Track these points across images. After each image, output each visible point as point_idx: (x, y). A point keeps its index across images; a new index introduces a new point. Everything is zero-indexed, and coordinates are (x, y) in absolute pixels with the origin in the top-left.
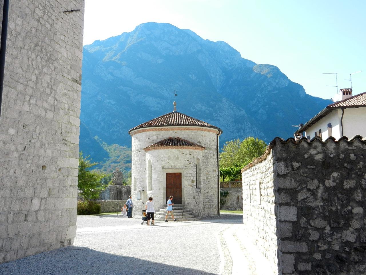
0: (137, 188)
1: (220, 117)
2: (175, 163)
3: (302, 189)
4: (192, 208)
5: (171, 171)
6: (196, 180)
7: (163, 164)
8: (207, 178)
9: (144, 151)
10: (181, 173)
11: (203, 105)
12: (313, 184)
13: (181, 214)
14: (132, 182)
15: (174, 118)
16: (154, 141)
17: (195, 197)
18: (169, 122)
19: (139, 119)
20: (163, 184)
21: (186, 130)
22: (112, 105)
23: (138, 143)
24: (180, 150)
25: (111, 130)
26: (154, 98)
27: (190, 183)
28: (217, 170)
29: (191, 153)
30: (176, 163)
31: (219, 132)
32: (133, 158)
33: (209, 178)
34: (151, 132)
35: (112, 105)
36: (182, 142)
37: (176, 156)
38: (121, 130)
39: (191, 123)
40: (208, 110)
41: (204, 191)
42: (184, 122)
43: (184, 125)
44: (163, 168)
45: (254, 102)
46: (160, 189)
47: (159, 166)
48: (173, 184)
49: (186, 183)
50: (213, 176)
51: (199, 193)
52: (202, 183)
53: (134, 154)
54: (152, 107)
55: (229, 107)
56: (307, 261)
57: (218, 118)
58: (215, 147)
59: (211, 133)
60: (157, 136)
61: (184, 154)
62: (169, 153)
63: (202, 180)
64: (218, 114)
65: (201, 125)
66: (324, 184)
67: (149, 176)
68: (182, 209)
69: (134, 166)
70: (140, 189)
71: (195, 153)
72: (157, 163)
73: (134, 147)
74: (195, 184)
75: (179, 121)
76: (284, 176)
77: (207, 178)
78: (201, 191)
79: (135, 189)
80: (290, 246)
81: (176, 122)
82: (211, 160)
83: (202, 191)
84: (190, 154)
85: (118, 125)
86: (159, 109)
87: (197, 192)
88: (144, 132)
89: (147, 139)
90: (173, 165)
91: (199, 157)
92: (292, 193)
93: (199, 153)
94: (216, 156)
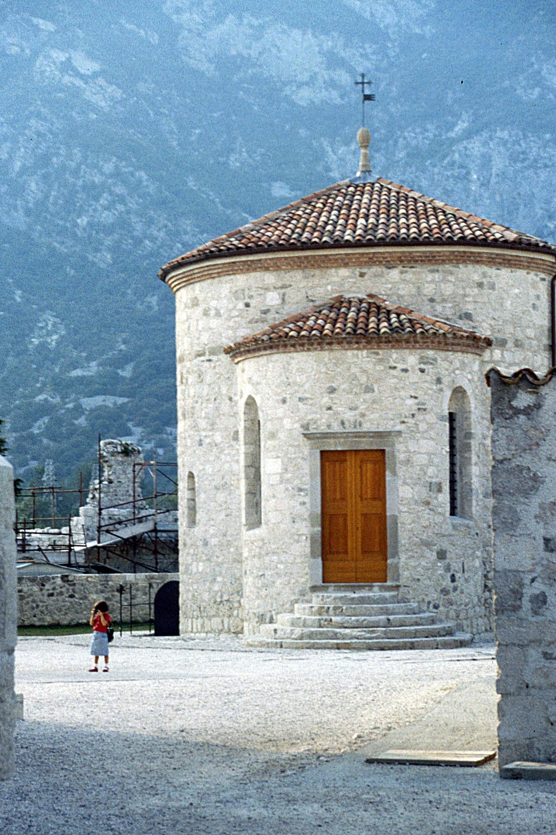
2: (356, 408)
6: (453, 482)
9: (225, 358)
10: (384, 451)
14: (180, 494)
16: (270, 316)
20: (307, 500)
21: (409, 261)
22: (82, 77)
23: (200, 323)
24: (380, 352)
25: (83, 221)
26: (310, 32)
30: (362, 408)
32: (183, 387)
34: (258, 274)
35: (82, 77)
38: (134, 219)
43: (396, 242)
47: (287, 424)
53: (184, 371)
54: (300, 85)
59: (521, 273)
61: (395, 368)
69: (188, 422)
71: (446, 365)
72: (281, 411)
73: (186, 340)
84: (422, 371)
85: (120, 190)
86: (342, 97)
89: (241, 305)
90: (349, 416)
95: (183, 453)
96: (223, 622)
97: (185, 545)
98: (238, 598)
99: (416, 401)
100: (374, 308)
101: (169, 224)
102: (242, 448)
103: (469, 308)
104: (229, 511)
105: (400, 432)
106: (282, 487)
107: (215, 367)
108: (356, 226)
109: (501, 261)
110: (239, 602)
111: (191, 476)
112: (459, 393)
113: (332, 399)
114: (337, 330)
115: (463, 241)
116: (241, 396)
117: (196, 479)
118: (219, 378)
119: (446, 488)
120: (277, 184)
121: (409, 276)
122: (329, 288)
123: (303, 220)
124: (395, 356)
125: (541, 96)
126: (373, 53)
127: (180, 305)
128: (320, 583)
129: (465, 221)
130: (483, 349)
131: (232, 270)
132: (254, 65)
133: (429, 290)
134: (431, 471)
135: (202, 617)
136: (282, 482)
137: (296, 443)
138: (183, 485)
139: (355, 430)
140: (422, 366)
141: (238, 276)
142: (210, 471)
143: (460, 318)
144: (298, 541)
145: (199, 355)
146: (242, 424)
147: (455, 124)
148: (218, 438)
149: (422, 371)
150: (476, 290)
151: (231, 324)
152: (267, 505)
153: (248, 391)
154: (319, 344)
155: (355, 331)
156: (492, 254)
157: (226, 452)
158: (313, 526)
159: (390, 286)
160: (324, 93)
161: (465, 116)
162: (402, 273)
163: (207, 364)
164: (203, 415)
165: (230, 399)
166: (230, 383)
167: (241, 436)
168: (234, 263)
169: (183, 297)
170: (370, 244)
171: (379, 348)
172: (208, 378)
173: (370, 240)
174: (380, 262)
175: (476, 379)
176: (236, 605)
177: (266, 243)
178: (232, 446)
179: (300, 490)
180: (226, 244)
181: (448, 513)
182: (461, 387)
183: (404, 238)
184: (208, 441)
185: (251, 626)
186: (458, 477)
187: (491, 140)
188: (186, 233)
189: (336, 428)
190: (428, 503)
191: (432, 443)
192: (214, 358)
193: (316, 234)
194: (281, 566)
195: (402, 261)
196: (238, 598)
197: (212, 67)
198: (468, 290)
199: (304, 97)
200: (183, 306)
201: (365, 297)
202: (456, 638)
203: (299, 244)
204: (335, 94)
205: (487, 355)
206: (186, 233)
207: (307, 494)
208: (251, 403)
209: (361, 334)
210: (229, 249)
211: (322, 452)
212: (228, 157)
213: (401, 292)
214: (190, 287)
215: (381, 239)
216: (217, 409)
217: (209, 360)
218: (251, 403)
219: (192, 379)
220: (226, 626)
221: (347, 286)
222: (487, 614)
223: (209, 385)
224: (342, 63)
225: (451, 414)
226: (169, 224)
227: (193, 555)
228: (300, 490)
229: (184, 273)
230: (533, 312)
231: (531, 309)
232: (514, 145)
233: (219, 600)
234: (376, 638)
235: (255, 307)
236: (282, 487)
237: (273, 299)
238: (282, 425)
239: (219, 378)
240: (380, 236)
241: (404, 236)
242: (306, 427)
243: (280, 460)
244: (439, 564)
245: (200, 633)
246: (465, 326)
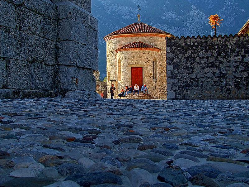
3: (176, 58)
11: (173, 13)
12: (180, 56)
13: (142, 96)
15: (138, 27)
18: (134, 30)
36: (143, 45)
39: (150, 31)
42: (145, 30)
43: (144, 32)
44: (129, 64)
45: (223, 9)
49: (146, 75)
55: (198, 14)
56: (176, 86)
57: (188, 25)
62: (134, 53)
66: (184, 56)
75: (141, 30)
76: (169, 53)
80: (170, 80)
81: (139, 30)
84: (149, 54)
89: (118, 43)
92: (172, 60)
93: (156, 54)
119: (153, 74)
125: (166, 18)
127: (107, 43)
133: (150, 41)
138: (107, 74)
149: (149, 54)
186: (155, 72)
198: (157, 41)
199: (125, 18)
208: (119, 59)
211: (132, 68)
224: (132, 12)
237: (123, 42)
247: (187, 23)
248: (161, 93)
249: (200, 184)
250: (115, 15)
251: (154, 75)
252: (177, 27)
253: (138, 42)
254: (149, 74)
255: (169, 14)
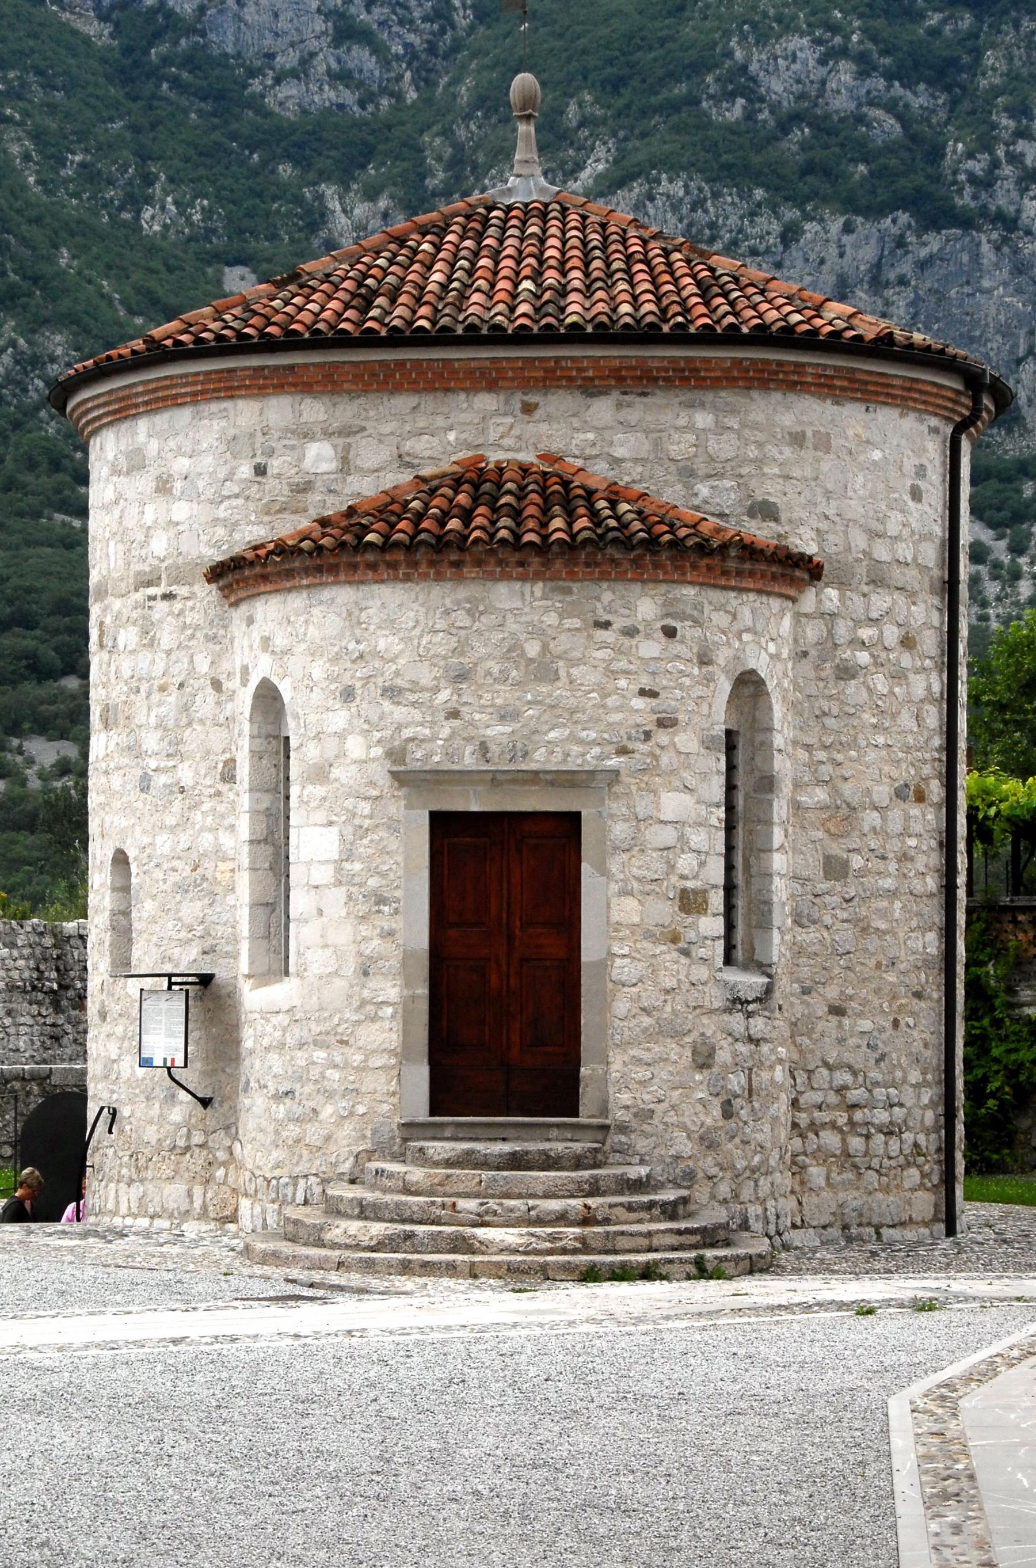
0: (144, 955)
1: (1019, 181)
4: (677, 1158)
5: (474, 802)
6: (730, 889)
7: (399, 728)
8: (835, 868)
9: (207, 593)
10: (578, 815)
11: (843, 52)
16: (314, 498)
17: (711, 1055)
19: (147, 213)
23: (149, 510)
27: (664, 911)
28: (936, 790)
29: (683, 617)
31: (976, 401)
32: (105, 656)
33: (857, 862)
37: (533, 649)
40: (891, 107)
41: (806, 991)
46: (366, 974)
47: (356, 747)
48: (501, 936)
49: (628, 910)
50: (894, 846)
51: (749, 1015)
52: (781, 916)
57: (1003, 198)
58: (931, 554)
60: (340, 441)
63: (780, 890)
64: (1000, 153)
65: (789, 329)
67: (548, 1157)
68: (578, 1163)
70: (168, 968)
71: (721, 619)
72: (339, 719)
74: (713, 925)
77: (835, 868)
78: (769, 990)
79: (122, 967)
82: (880, 683)
83: (785, 986)
84: (670, 633)
87: (737, 1003)
88: (215, 407)
89: (246, 470)
90: (497, 731)
91: (759, 662)
93: (761, 631)
94: (931, 643)
95: (102, 806)
96: (190, 1195)
97: (103, 1015)
98: (227, 1142)
99: (654, 702)
100: (557, 488)
101: (21, 341)
102: (242, 798)
103: (770, 490)
104: (209, 942)
105: (615, 774)
106: (341, 893)
107: (181, 613)
108: (514, 296)
109: (846, 384)
110: (230, 1150)
111: (121, 860)
112: (748, 686)
113: (459, 693)
114: (477, 534)
115: (762, 336)
116: (244, 683)
117: (134, 868)
118: (192, 637)
119: (717, 900)
120: (239, 270)
121: (632, 415)
122: (452, 436)
123: (390, 279)
124: (607, 597)
125: (750, 116)
126: (425, 19)
127: (99, 468)
128: (421, 1112)
129: (762, 292)
130: (800, 585)
131: (226, 388)
132: (191, 30)
133: (680, 446)
134: (686, 862)
135: (142, 1181)
136: (338, 883)
137: (375, 793)
139: (512, 767)
140: (670, 622)
141: (241, 404)
142: (166, 850)
143: (752, 513)
144: (374, 1018)
145: (149, 584)
146: (245, 743)
147: (579, 167)
148: (186, 774)
150: (787, 451)
151: (222, 512)
152: (301, 935)
153: (263, 668)
154: (432, 564)
155: (517, 537)
156: (825, 367)
157: (206, 807)
158: (407, 984)
159: (591, 436)
160: (330, 94)
161: (600, 151)
162: (619, 406)
163: (162, 606)
164: (153, 720)
165: (217, 685)
166: (218, 647)
167: (243, 770)
168: (230, 371)
169: (106, 451)
170: (549, 337)
171: (572, 576)
172: (166, 638)
173: (548, 326)
174: (570, 379)
175: (785, 653)
176: (222, 1155)
177: (308, 328)
178: (218, 794)
179: (381, 900)
180: (214, 326)
181: (719, 961)
182: (753, 672)
183: (626, 326)
184: (162, 780)
185: (258, 1209)
186: (740, 878)
187: (652, 198)
188: (53, 360)
189: (469, 760)
190: (675, 939)
191: (686, 798)
192: (182, 591)
193: (424, 311)
194: (333, 1074)
195: (621, 380)
196: (227, 1142)
197: (107, 29)
198: (772, 451)
199: (287, 98)
200: (105, 471)
201: (535, 461)
202: (741, 1251)
203: (383, 333)
204: (349, 97)
205: (809, 600)
206: (53, 360)
207: (396, 912)
208: (268, 699)
209: (531, 543)
210: (220, 338)
212: (138, 212)
213: (619, 452)
214: (124, 426)
215: (574, 325)
216: (186, 708)
217: (168, 597)
218: (268, 699)
219: (128, 637)
220: (197, 1204)
221: (493, 435)
222: (797, 1188)
223: (169, 653)
225: (729, 733)
226: (21, 341)
227: (123, 1039)
228: (381, 900)
229: (110, 392)
230: (910, 503)
231: (907, 498)
232: (693, 210)
233: (181, 1143)
234: (564, 1251)
235: (279, 476)
236: (341, 893)
238: (340, 747)
239: (192, 637)
240: (574, 318)
241: (628, 320)
242: (396, 754)
243: (335, 830)
244: (698, 1077)
245: (135, 1216)
246: (761, 532)
247: (995, 164)
248: (822, 1155)
249: (125, 923)
250: (166, 61)
251: (729, 908)
252: (875, 211)
253: (525, 470)
254: (665, 912)
255: (789, 66)
